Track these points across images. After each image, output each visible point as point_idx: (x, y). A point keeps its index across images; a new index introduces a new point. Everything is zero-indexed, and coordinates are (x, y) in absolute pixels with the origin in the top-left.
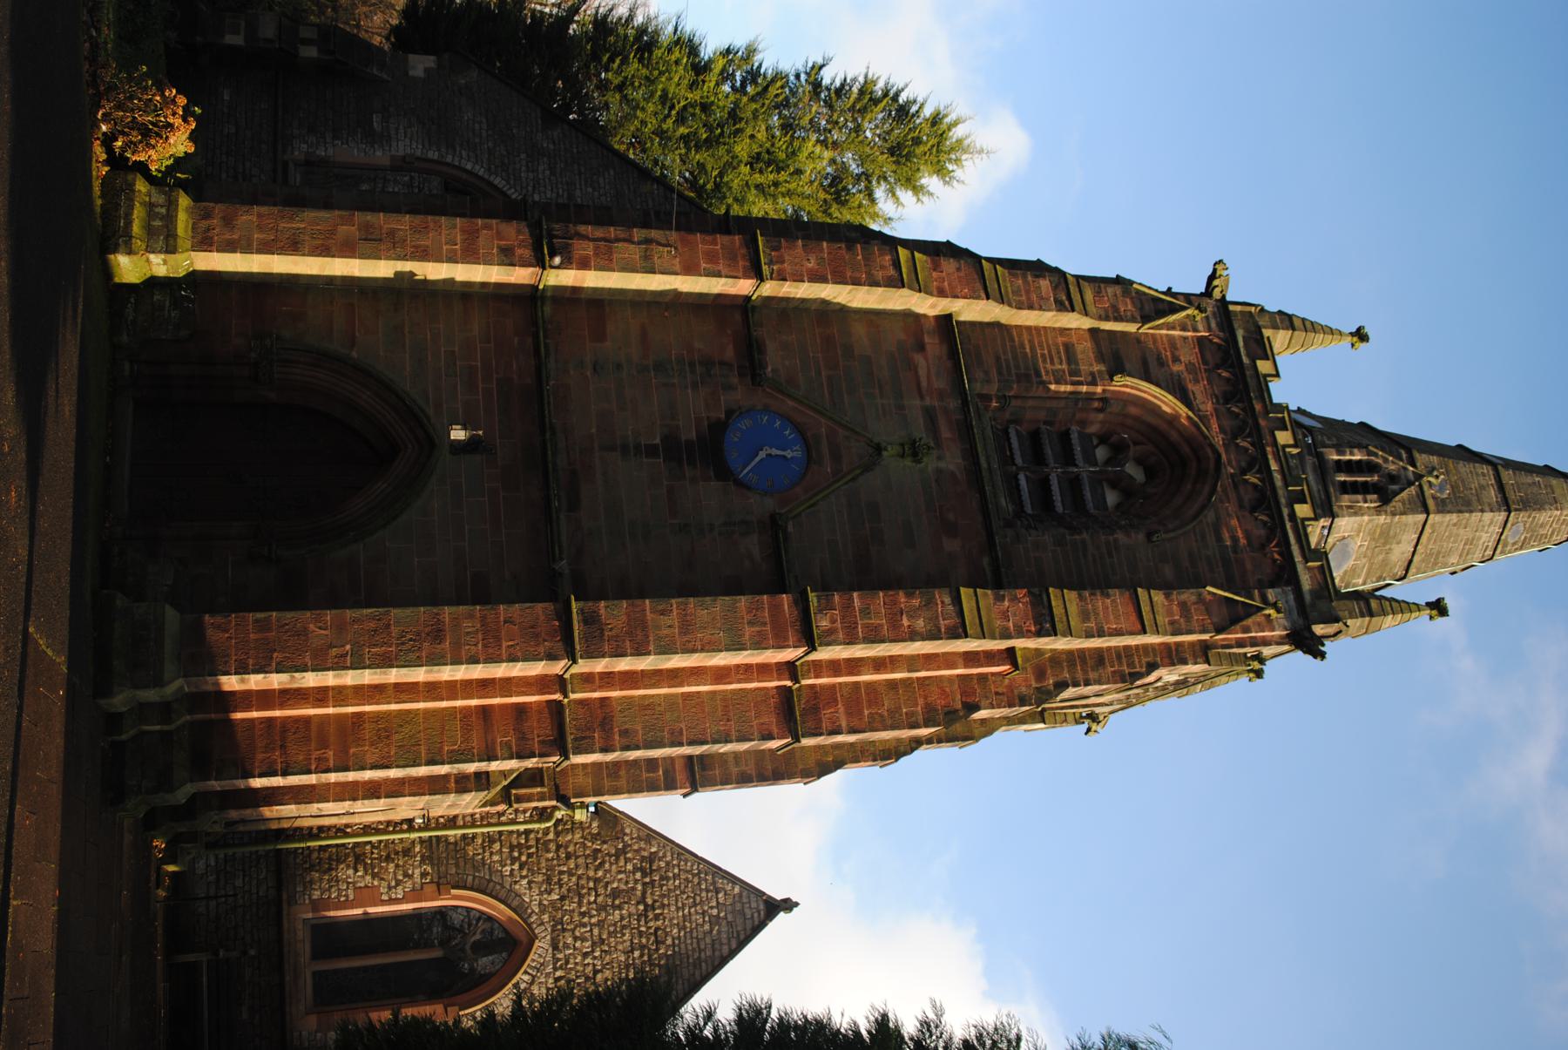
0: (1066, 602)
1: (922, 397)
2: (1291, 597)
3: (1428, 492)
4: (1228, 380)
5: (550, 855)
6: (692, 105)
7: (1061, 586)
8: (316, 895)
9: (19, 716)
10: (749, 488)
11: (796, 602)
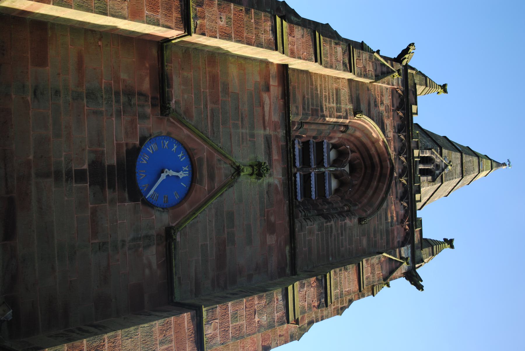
1: (265, 129)
2: (410, 251)
11: (192, 318)
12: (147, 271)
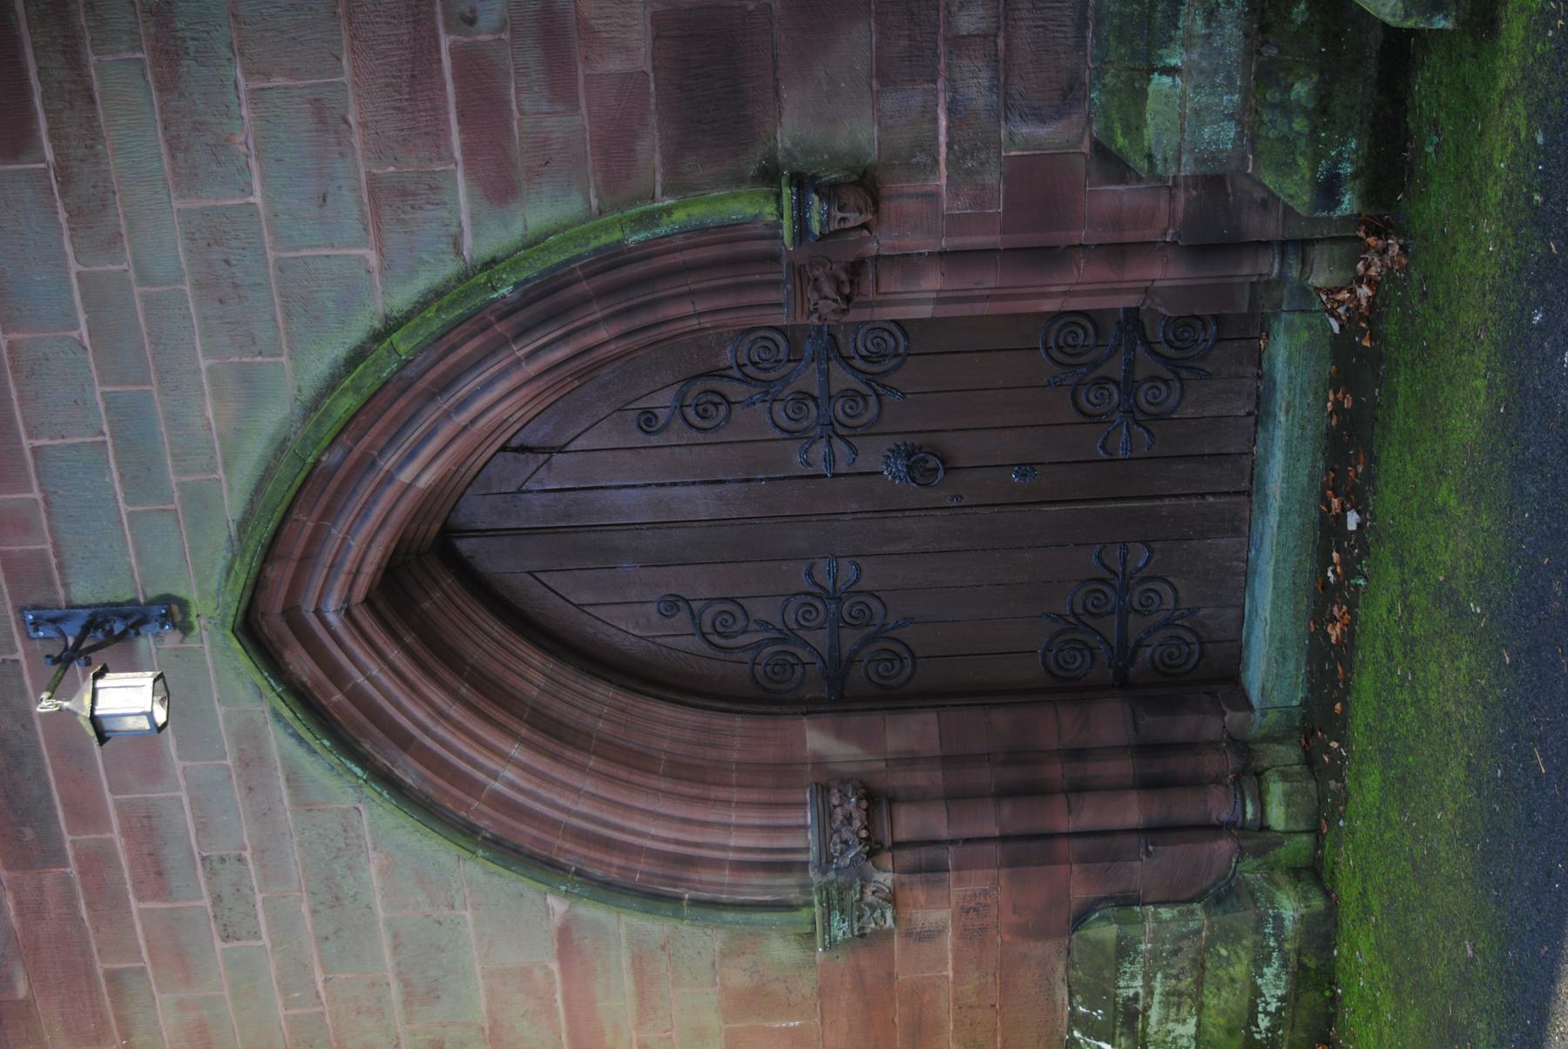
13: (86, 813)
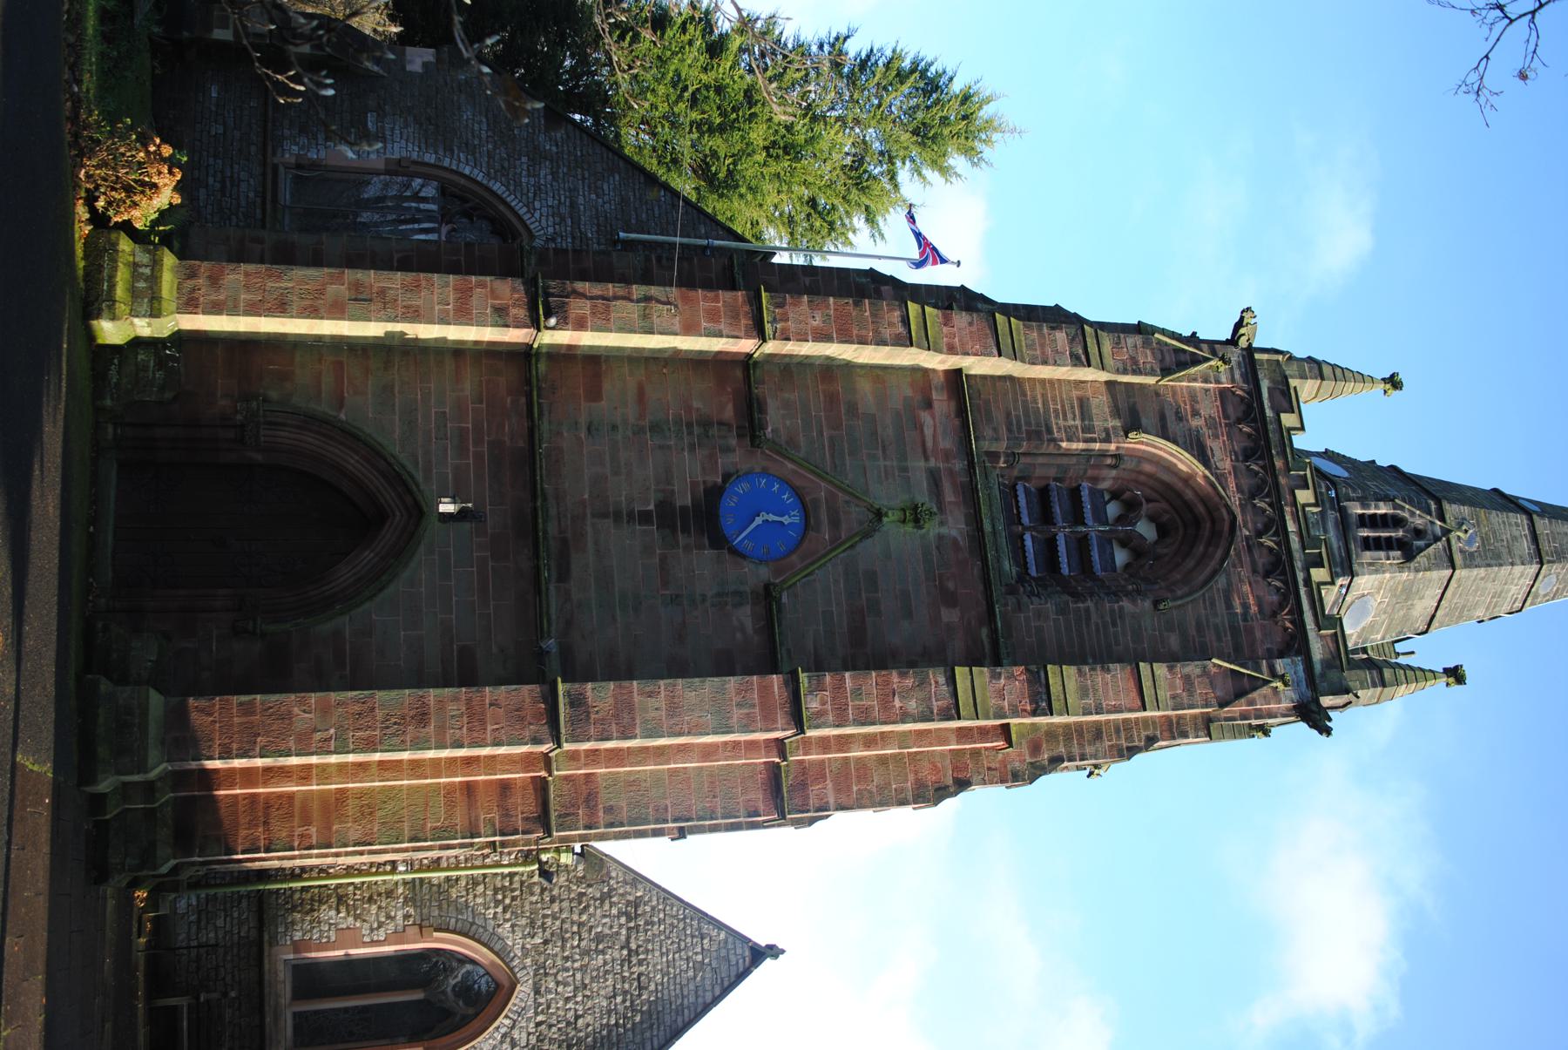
0: (1065, 679)
1: (927, 459)
3: (1455, 546)
4: (1249, 435)
5: (534, 899)
6: (707, 87)
7: (1061, 661)
8: (298, 936)
9: (9, 849)
10: (744, 557)
11: (786, 683)
12: (739, 635)
13: (478, 457)
